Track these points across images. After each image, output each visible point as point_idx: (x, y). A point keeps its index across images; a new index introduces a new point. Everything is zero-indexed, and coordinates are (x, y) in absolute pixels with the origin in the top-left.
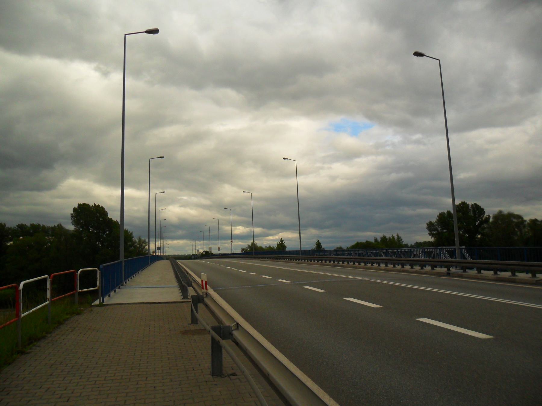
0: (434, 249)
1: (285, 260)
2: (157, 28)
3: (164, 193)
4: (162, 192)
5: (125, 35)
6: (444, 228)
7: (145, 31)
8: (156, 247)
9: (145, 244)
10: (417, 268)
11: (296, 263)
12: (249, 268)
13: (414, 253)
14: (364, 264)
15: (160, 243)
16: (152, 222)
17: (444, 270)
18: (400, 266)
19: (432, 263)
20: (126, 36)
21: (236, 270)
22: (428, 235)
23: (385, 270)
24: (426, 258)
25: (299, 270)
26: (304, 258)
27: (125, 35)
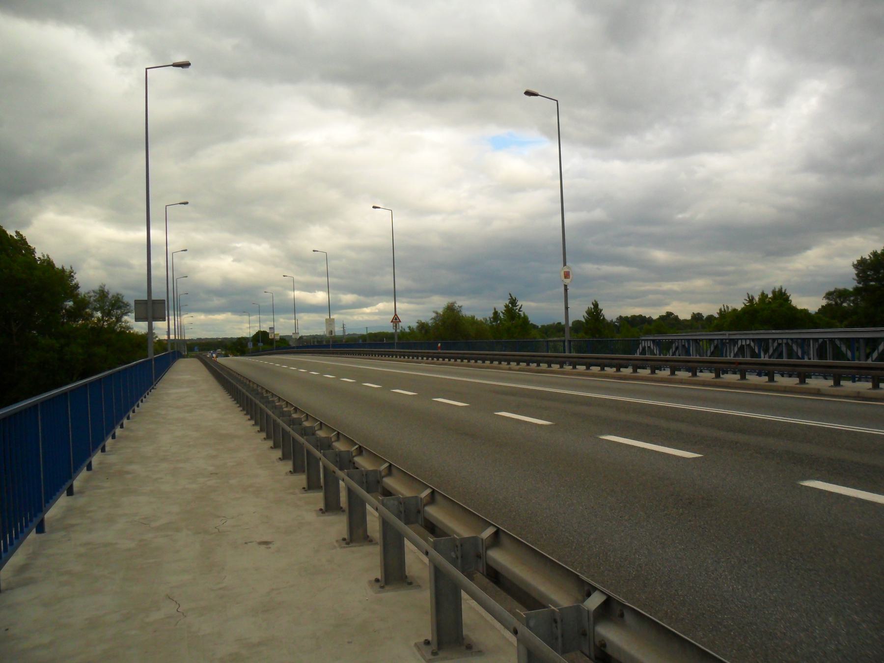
0: (680, 341)
1: (406, 357)
2: (187, 60)
3: (186, 252)
4: (182, 251)
5: (147, 69)
6: (750, 298)
7: (172, 64)
8: (167, 321)
9: (119, 308)
10: (568, 368)
11: (519, 370)
12: (324, 370)
13: (677, 344)
14: (546, 365)
15: (176, 319)
16: (159, 272)
17: (793, 381)
18: (648, 371)
19: (653, 363)
20: (148, 70)
21: (316, 375)
22: (720, 308)
23: (571, 374)
24: (549, 351)
25: (440, 376)
26: (408, 354)
27: (147, 69)
